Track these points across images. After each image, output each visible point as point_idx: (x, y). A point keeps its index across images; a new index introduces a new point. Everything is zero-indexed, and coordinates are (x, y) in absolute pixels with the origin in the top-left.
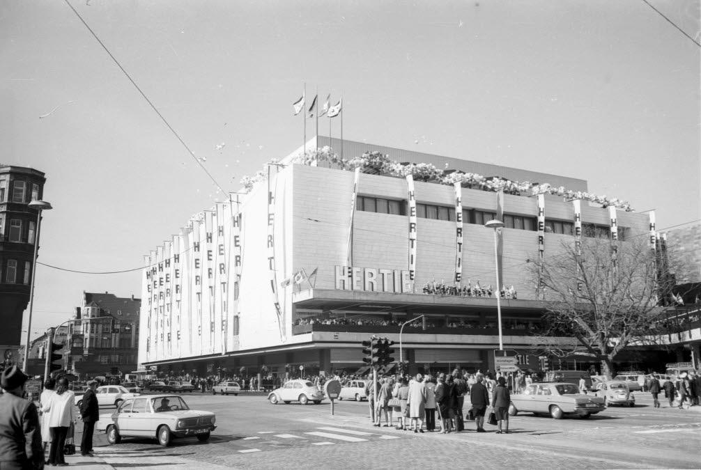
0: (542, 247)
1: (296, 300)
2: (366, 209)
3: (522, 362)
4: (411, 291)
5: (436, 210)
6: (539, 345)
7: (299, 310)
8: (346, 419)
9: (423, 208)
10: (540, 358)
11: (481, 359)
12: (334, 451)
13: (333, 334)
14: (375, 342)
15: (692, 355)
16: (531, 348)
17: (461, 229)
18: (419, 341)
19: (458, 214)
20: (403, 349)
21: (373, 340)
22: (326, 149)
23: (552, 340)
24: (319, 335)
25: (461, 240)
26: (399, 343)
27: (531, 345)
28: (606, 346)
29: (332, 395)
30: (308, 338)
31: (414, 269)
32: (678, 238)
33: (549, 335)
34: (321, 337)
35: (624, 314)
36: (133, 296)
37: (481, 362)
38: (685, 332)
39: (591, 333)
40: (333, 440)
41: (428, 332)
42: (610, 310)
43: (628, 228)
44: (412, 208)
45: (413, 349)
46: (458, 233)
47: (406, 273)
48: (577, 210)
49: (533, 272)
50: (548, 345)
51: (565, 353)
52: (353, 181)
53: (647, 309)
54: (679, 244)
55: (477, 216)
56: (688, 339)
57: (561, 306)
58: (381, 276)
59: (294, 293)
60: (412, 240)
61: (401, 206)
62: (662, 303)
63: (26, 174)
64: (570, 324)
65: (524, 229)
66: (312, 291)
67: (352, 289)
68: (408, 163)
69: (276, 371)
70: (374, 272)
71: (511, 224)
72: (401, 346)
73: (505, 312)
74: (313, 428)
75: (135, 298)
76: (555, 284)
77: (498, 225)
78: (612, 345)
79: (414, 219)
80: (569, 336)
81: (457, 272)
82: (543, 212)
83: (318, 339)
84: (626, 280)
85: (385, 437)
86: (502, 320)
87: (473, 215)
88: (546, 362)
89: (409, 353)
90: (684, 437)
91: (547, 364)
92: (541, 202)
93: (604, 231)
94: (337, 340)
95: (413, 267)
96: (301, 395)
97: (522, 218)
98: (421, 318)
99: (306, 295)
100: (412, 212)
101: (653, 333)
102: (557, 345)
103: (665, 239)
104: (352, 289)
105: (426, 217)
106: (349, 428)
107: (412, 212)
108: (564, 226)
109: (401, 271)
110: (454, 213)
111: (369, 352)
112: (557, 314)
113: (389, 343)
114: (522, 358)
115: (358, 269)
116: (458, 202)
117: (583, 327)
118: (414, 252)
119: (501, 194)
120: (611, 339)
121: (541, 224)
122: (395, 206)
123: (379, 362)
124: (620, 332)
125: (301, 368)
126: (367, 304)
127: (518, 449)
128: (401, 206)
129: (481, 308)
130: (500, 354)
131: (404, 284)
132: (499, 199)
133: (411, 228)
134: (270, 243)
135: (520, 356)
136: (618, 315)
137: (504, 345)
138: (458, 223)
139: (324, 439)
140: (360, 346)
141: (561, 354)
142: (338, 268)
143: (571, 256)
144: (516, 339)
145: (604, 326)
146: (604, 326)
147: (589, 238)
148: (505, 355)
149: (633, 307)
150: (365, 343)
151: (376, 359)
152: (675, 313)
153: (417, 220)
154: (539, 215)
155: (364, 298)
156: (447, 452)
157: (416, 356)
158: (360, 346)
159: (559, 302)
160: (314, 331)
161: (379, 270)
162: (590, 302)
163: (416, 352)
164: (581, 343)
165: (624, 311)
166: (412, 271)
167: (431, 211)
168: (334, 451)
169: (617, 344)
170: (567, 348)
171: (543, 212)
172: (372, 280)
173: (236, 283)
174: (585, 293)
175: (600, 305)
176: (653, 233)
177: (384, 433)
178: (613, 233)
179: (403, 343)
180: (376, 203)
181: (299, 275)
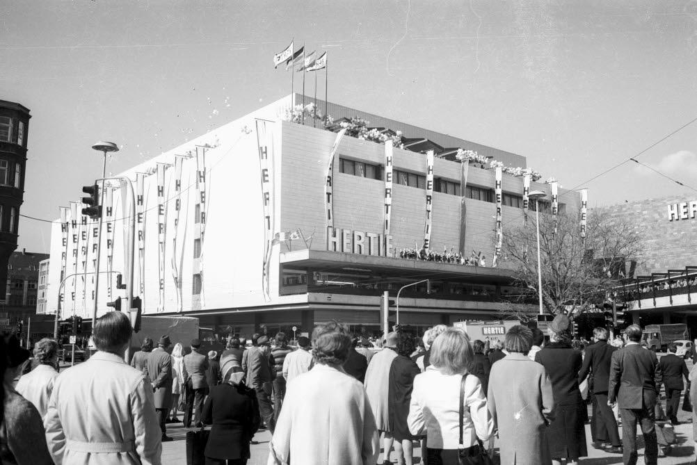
1: (283, 261)
4: (392, 255)
17: (430, 197)
20: (400, 312)
25: (430, 207)
34: (316, 299)
36: (24, 249)
38: (633, 302)
43: (565, 204)
52: (331, 144)
59: (282, 252)
61: (377, 171)
63: (13, 110)
69: (239, 332)
70: (363, 235)
75: (26, 251)
79: (389, 185)
81: (426, 238)
83: (313, 300)
87: (440, 184)
91: (577, 329)
92: (499, 176)
95: (428, 236)
98: (426, 283)
99: (302, 255)
104: (343, 251)
107: (388, 177)
109: (342, 230)
115: (348, 232)
118: (388, 217)
119: (466, 165)
121: (389, 175)
126: (358, 267)
128: (377, 171)
129: (379, 268)
131: (345, 243)
132: (463, 170)
133: (387, 193)
160: (309, 292)
163: (315, 313)
166: (427, 240)
172: (360, 242)
173: (198, 241)
178: (497, 195)
180: (354, 165)
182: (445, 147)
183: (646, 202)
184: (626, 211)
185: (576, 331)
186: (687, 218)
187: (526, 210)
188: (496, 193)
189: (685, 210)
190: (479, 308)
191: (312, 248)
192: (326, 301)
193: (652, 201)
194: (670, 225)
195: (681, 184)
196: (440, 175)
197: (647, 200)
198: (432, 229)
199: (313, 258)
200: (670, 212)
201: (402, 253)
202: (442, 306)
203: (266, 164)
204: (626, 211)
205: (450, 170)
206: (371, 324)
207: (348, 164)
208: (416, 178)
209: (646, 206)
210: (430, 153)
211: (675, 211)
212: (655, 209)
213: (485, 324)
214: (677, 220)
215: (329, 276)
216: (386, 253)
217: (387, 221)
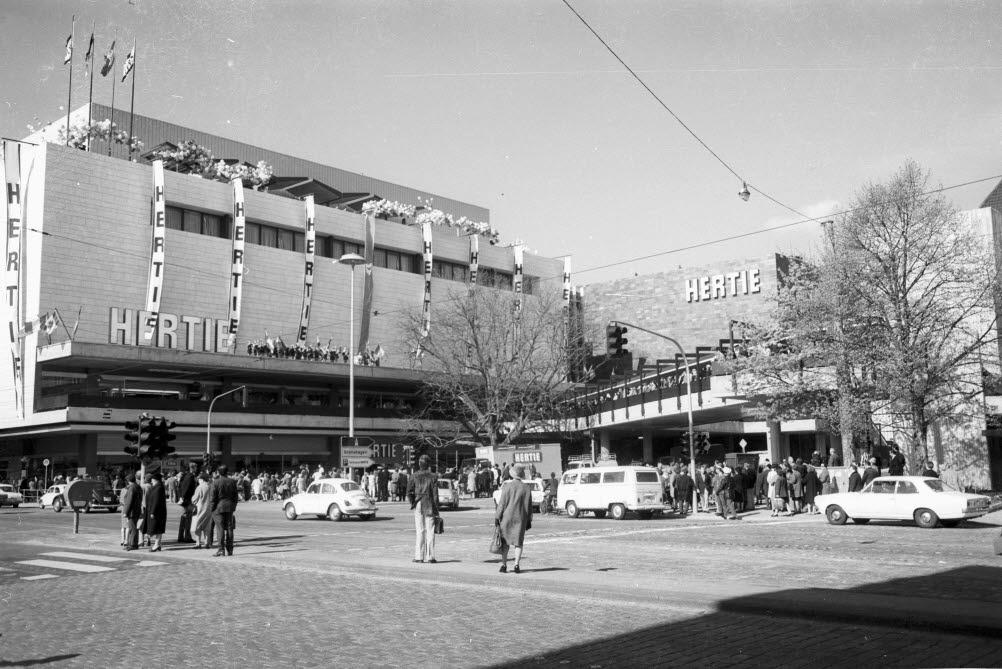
0: (310, 279)
2: (185, 227)
3: (381, 453)
4: (226, 348)
5: (180, 214)
6: (410, 431)
7: (46, 374)
8: (94, 538)
9: (256, 231)
10: (405, 447)
11: (330, 450)
12: (53, 588)
13: (102, 411)
14: (146, 424)
15: (593, 445)
16: (399, 434)
17: (311, 264)
18: (237, 423)
19: (309, 241)
20: (211, 434)
21: (142, 420)
22: (105, 125)
23: (428, 424)
24: (77, 413)
25: (310, 279)
26: (206, 426)
27: (398, 430)
28: (498, 433)
29: (76, 504)
30: (59, 416)
31: (238, 318)
32: (598, 294)
33: (423, 418)
34: (81, 414)
35: (522, 391)
37: (328, 453)
39: (480, 416)
40: (57, 571)
41: (251, 409)
42: (506, 386)
44: (238, 228)
45: (229, 435)
46: (307, 269)
47: (224, 323)
48: (428, 237)
49: (408, 329)
50: (422, 431)
51: (443, 442)
53: (550, 385)
54: (598, 302)
55: (337, 248)
56: (597, 425)
57: (440, 378)
58: (185, 326)
59: (40, 347)
60: (236, 275)
61: (222, 225)
62: (572, 377)
64: (451, 404)
65: (400, 269)
66: (68, 345)
67: (110, 342)
68: (236, 161)
70: (174, 319)
71: (199, 228)
72: (209, 430)
73: (361, 383)
74: (35, 553)
76: (437, 348)
77: (358, 262)
78: (505, 432)
79: (240, 245)
80: (451, 419)
82: (242, 210)
83: (76, 418)
84: (528, 346)
85: (144, 564)
86: (355, 394)
87: (329, 245)
88: (413, 454)
89: (222, 441)
90: (557, 548)
92: (428, 237)
93: (505, 279)
94: (108, 420)
95: (237, 315)
96: (332, 506)
97: (399, 254)
99: (60, 351)
100: (238, 233)
101: (556, 416)
102: (433, 431)
103: (582, 295)
105: (260, 244)
106: (101, 553)
107: (238, 233)
108: (186, 215)
109: (217, 321)
110: (304, 241)
111: (135, 439)
112: (436, 389)
113: (169, 424)
114: (387, 448)
116: (309, 224)
117: (470, 407)
118: (238, 292)
120: (505, 424)
121: (240, 230)
122: (213, 224)
123: (150, 454)
124: (516, 415)
125: (46, 463)
127: (332, 573)
128: (222, 225)
129: (294, 376)
130: (348, 442)
133: (235, 257)
134: (13, 265)
135: (384, 446)
136: (515, 392)
137: (355, 430)
138: (307, 255)
139: (43, 570)
140: (123, 428)
141: (439, 444)
142: (114, 311)
143: (458, 311)
144: (380, 423)
145: (495, 406)
146: (495, 406)
147: (486, 289)
148: (357, 444)
149: (535, 383)
150: (129, 425)
151: (145, 449)
152: (585, 391)
153: (245, 247)
154: (425, 252)
155: (155, 358)
156: (227, 582)
157: (99, 444)
158: (123, 428)
159: (441, 374)
161: (182, 317)
162: (480, 373)
163: (234, 439)
164: (464, 429)
165: (523, 387)
167: (267, 234)
168: (53, 588)
169: (512, 429)
170: (446, 435)
171: (242, 210)
172: (169, 331)
174: (476, 362)
175: (493, 378)
176: (567, 285)
177: (145, 558)
179: (212, 426)
180: (183, 213)
181: (51, 318)
182: (343, 191)
183: (660, 276)
184: (635, 288)
185: (412, 459)
186: (709, 299)
187: (429, 276)
188: (426, 260)
189: (707, 288)
190: (375, 427)
191: (76, 340)
192: (101, 419)
193: (669, 274)
194: (688, 308)
195: (92, 41)
196: (328, 231)
197: (661, 273)
198: (243, 302)
199: (75, 353)
200: (688, 290)
201: (250, 346)
202: (311, 425)
203: (16, 210)
204: (635, 288)
205: (342, 222)
206: (305, 453)
207: (180, 216)
208: (287, 237)
209: (660, 281)
210: (310, 199)
211: (694, 289)
212: (671, 285)
213: (517, 448)
214: (697, 301)
215: (128, 381)
216: (216, 347)
217: (235, 298)
